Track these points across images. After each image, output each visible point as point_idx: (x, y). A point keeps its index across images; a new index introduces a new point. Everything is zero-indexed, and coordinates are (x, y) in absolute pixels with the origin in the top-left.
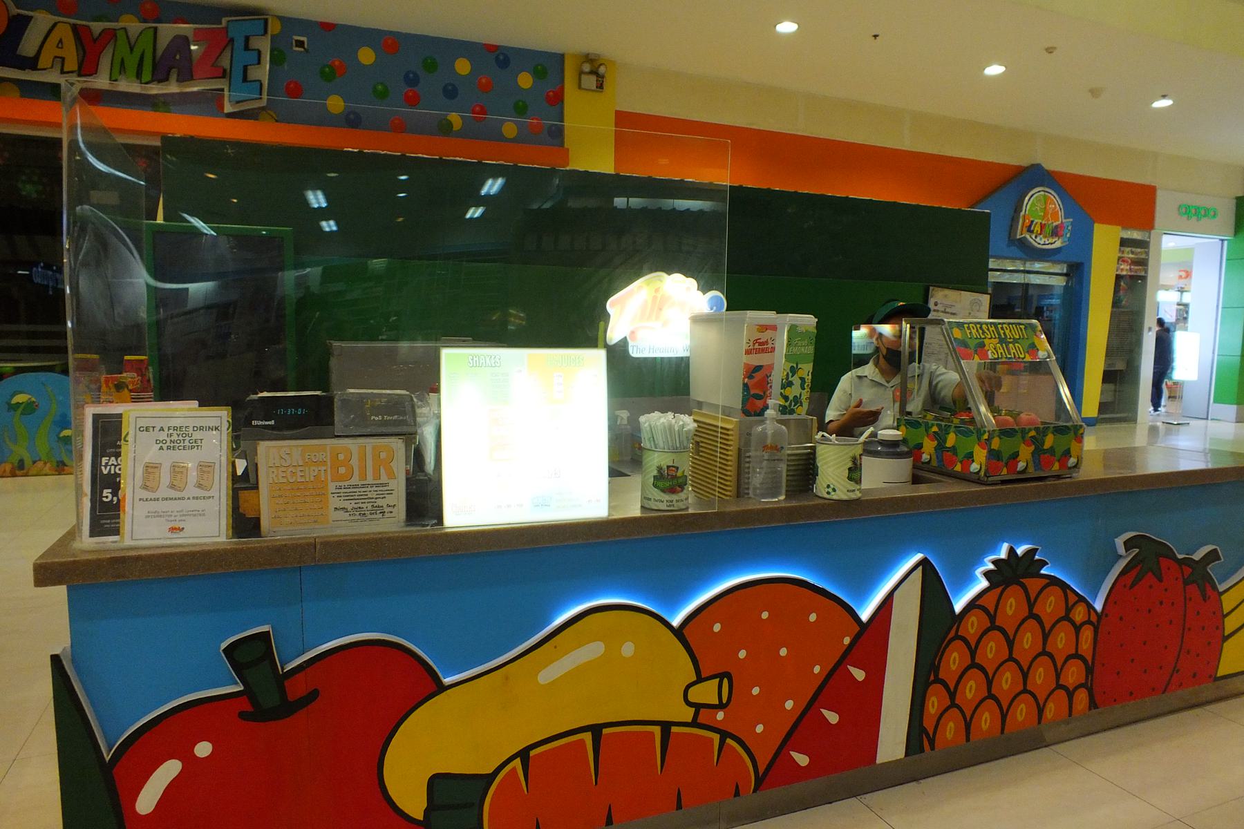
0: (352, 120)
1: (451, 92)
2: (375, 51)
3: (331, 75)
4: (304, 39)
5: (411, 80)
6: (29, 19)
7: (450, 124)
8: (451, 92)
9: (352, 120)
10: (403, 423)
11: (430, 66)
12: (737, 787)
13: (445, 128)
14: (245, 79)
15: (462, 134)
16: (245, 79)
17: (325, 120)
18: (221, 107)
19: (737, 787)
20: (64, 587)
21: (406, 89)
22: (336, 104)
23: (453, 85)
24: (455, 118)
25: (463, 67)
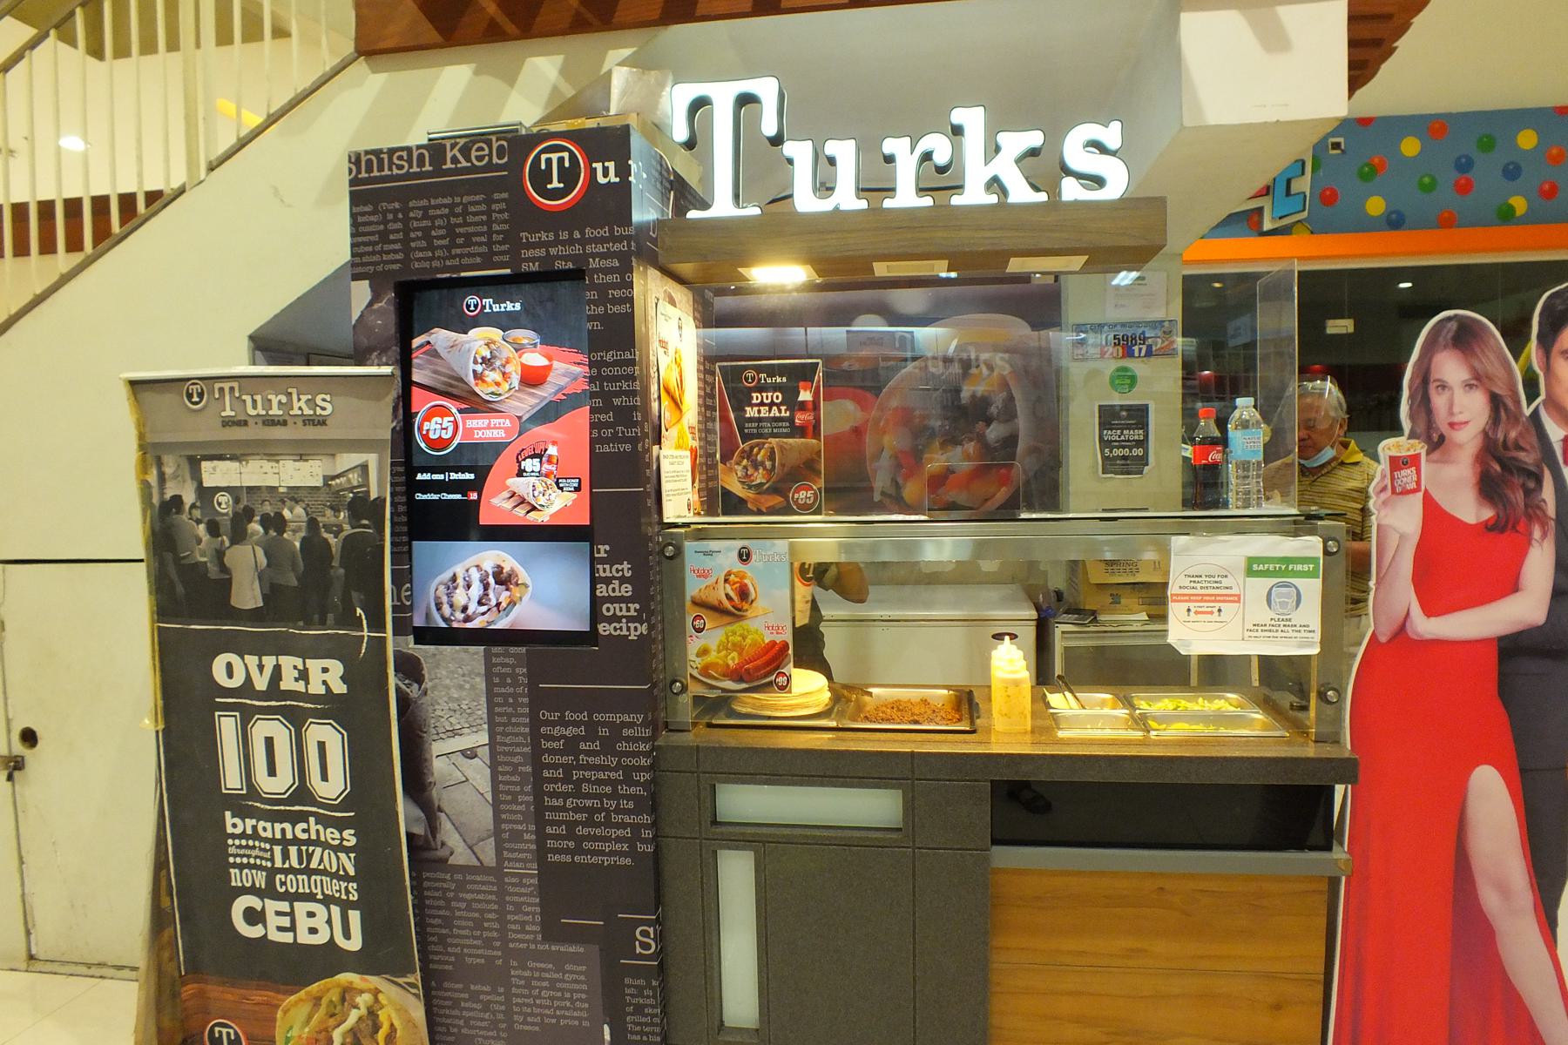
0: (1394, 221)
1: (1512, 172)
2: (1516, 145)
3: (1371, 173)
4: (1341, 140)
5: (1464, 165)
6: (75, 47)
7: (1512, 208)
8: (1512, 172)
9: (1394, 221)
10: (634, 393)
11: (1487, 144)
12: (133, 210)
13: (1506, 216)
14: (1288, 193)
15: (1527, 219)
16: (1288, 193)
17: (1365, 225)
18: (1261, 223)
19: (133, 210)
20: (261, 604)
21: (1455, 175)
22: (1376, 206)
23: (1466, 157)
24: (1519, 204)
25: (1527, 140)
